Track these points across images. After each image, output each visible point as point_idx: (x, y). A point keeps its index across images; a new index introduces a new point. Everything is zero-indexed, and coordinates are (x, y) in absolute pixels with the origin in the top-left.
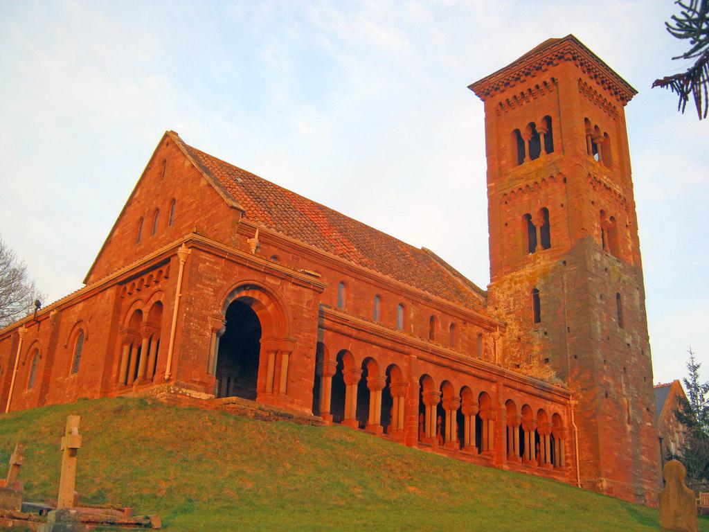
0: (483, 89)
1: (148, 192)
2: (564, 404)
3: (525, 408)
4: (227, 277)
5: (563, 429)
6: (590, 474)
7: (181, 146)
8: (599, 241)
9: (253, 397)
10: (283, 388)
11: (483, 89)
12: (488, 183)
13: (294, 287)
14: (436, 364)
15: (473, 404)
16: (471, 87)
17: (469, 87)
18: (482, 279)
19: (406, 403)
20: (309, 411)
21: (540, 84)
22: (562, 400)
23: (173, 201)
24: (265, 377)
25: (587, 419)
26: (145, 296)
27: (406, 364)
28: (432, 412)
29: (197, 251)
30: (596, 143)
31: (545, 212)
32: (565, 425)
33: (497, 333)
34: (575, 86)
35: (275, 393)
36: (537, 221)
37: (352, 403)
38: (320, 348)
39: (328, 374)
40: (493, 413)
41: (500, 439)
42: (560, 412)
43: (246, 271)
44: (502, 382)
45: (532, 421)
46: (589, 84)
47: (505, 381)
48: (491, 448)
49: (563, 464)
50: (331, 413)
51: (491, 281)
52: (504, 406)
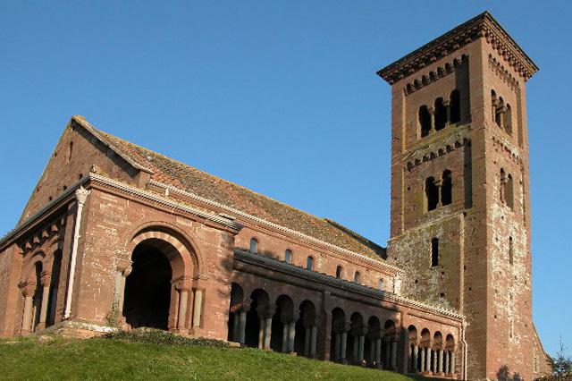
0: (391, 74)
3: (356, 316)
4: (133, 218)
11: (391, 74)
13: (207, 229)
14: (347, 298)
17: (381, 73)
19: (318, 332)
42: (453, 334)
44: (407, 311)
46: (498, 60)
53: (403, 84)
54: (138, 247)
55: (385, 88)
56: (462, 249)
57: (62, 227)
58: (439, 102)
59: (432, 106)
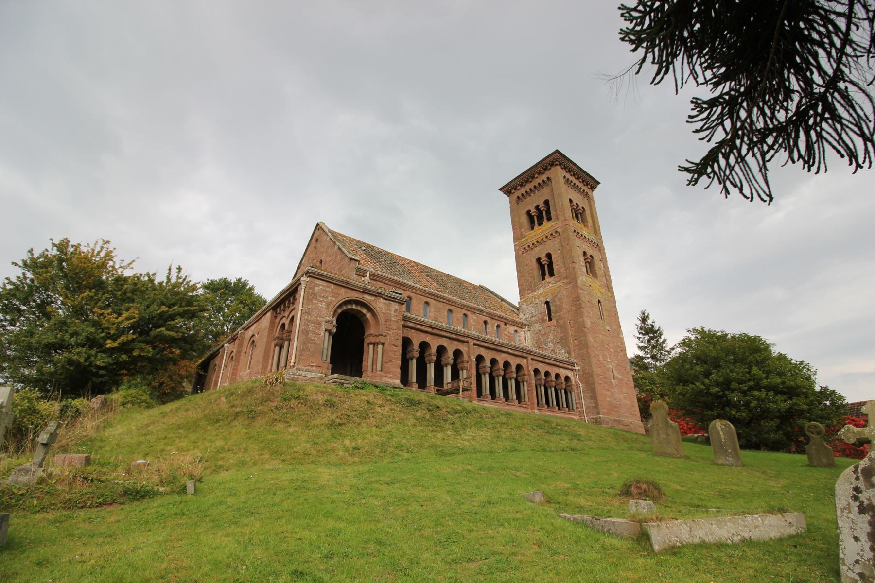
0: (508, 190)
1: (309, 259)
2: (572, 370)
3: (547, 374)
4: (336, 295)
5: (571, 385)
6: (593, 414)
7: (327, 231)
8: (584, 269)
9: (360, 377)
10: (379, 367)
11: (508, 190)
12: (514, 242)
15: (512, 372)
16: (500, 189)
17: (499, 190)
18: (511, 293)
20: (397, 382)
21: (541, 182)
22: (570, 367)
23: (321, 261)
24: (367, 363)
25: (588, 378)
26: (286, 314)
27: (466, 349)
28: (486, 380)
29: (314, 279)
30: (578, 214)
31: (549, 256)
32: (573, 383)
33: (526, 329)
34: (562, 180)
35: (374, 371)
36: (544, 260)
37: (430, 375)
38: (406, 343)
39: (446, 365)
40: (525, 377)
41: (532, 394)
43: (349, 291)
44: (530, 357)
45: (552, 381)
47: (532, 357)
48: (527, 400)
49: (575, 408)
50: (416, 383)
51: (520, 299)
52: (532, 373)
53: (515, 197)
54: (340, 314)
55: (506, 199)
56: (777, 28)
57: (295, 299)
58: (537, 207)
59: (533, 212)
